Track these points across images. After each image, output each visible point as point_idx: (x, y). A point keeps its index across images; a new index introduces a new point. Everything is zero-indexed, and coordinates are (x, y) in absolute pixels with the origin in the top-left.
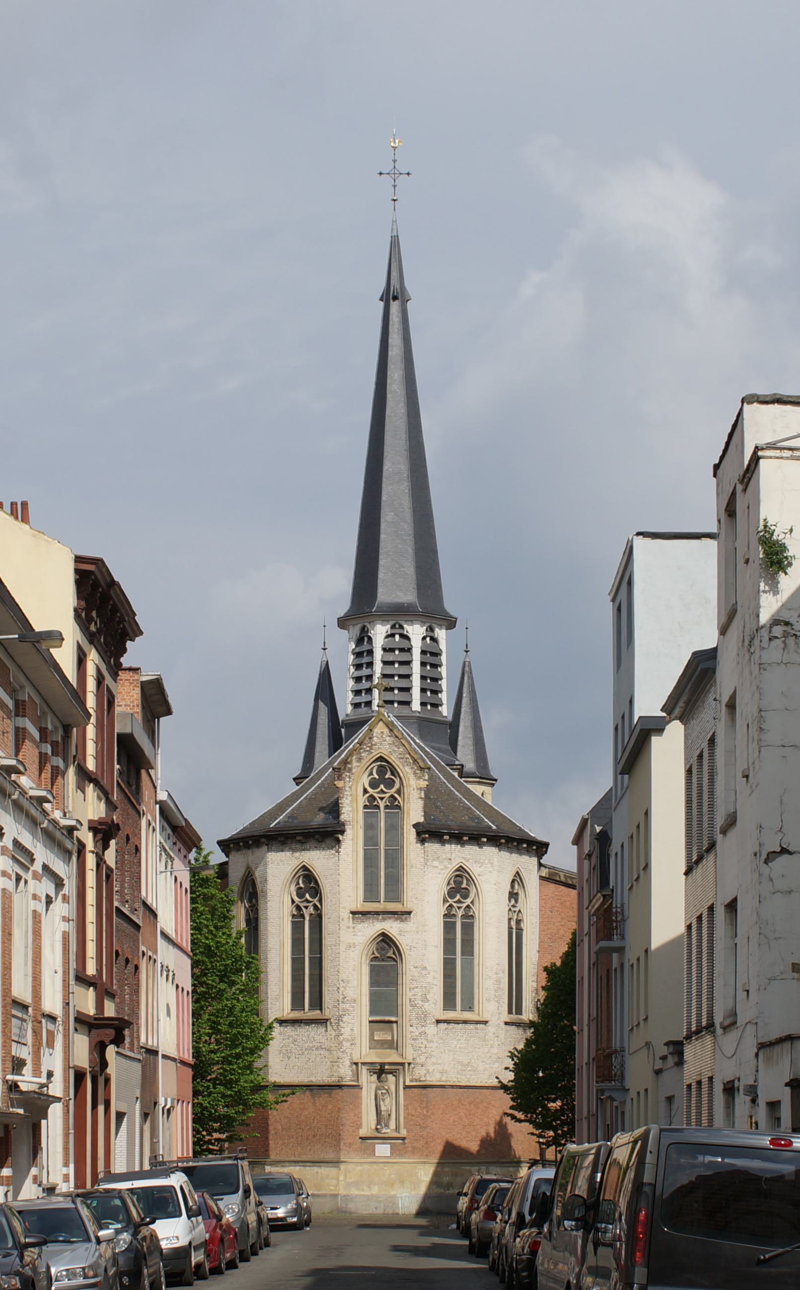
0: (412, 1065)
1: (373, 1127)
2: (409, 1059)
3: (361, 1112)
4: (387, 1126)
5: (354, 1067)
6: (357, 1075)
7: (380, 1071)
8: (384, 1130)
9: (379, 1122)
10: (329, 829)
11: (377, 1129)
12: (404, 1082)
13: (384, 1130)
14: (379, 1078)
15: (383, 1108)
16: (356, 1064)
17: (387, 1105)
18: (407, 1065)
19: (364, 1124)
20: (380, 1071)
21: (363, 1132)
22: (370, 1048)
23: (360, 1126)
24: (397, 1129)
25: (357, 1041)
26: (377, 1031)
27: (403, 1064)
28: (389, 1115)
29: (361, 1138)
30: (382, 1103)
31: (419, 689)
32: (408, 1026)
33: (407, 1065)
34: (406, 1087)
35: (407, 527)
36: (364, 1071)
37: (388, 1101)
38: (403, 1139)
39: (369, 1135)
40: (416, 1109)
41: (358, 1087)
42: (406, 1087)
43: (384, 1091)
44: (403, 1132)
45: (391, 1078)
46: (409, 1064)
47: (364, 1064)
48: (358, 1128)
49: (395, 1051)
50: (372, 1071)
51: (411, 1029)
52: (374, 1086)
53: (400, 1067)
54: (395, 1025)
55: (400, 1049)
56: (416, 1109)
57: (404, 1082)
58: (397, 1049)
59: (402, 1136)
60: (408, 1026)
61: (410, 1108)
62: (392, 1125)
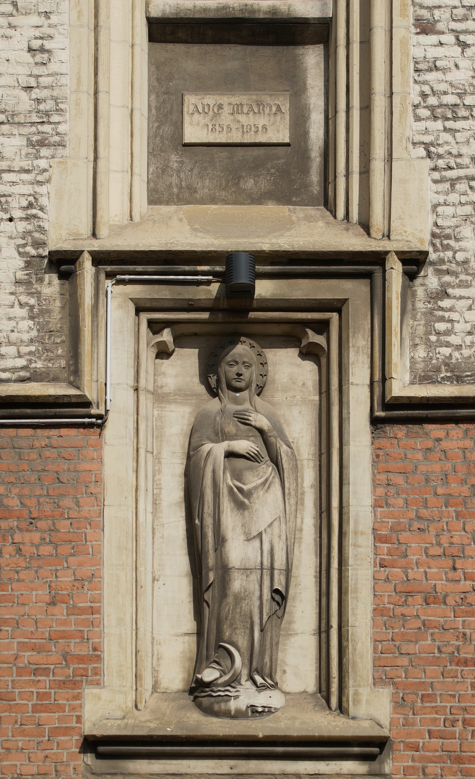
0: (430, 279)
1: (174, 677)
2: (412, 232)
3: (93, 580)
4: (263, 672)
5: (51, 286)
6: (71, 337)
7: (221, 313)
8: (246, 696)
9: (209, 641)
10: (43, 666)
11: (197, 689)
12: (380, 378)
13: (246, 696)
14: (213, 377)
15: (238, 551)
16: (63, 264)
17: (267, 528)
18: (395, 272)
19: (116, 655)
20: (221, 313)
21: (106, 707)
22: (155, 198)
23: (85, 667)
24: (331, 687)
25: (75, 126)
26: (203, 85)
27: (366, 265)
28: (280, 598)
29: (91, 744)
30: (230, 519)
31: (370, 608)
32: (404, 25)
33: (395, 272)
34: (393, 413)
35: (323, 554)
36: (116, 316)
37: (268, 505)
38: (371, 748)
39: (145, 723)
40: (454, 557)
41: (76, 414)
42: (393, 413)
43: (243, 445)
44: (372, 709)
45: (289, 369)
46: (414, 263)
47: (114, 263)
48: (73, 684)
49: (318, 211)
50: (168, 327)
51: (423, 47)
52: (177, 421)
53: (354, 291)
54: (312, 57)
55: (347, 189)
56: (454, 557)
57: (380, 378)
58: (328, 203)
59: (363, 729)
60: (404, 25)
61: (415, 547)
62: (298, 661)
